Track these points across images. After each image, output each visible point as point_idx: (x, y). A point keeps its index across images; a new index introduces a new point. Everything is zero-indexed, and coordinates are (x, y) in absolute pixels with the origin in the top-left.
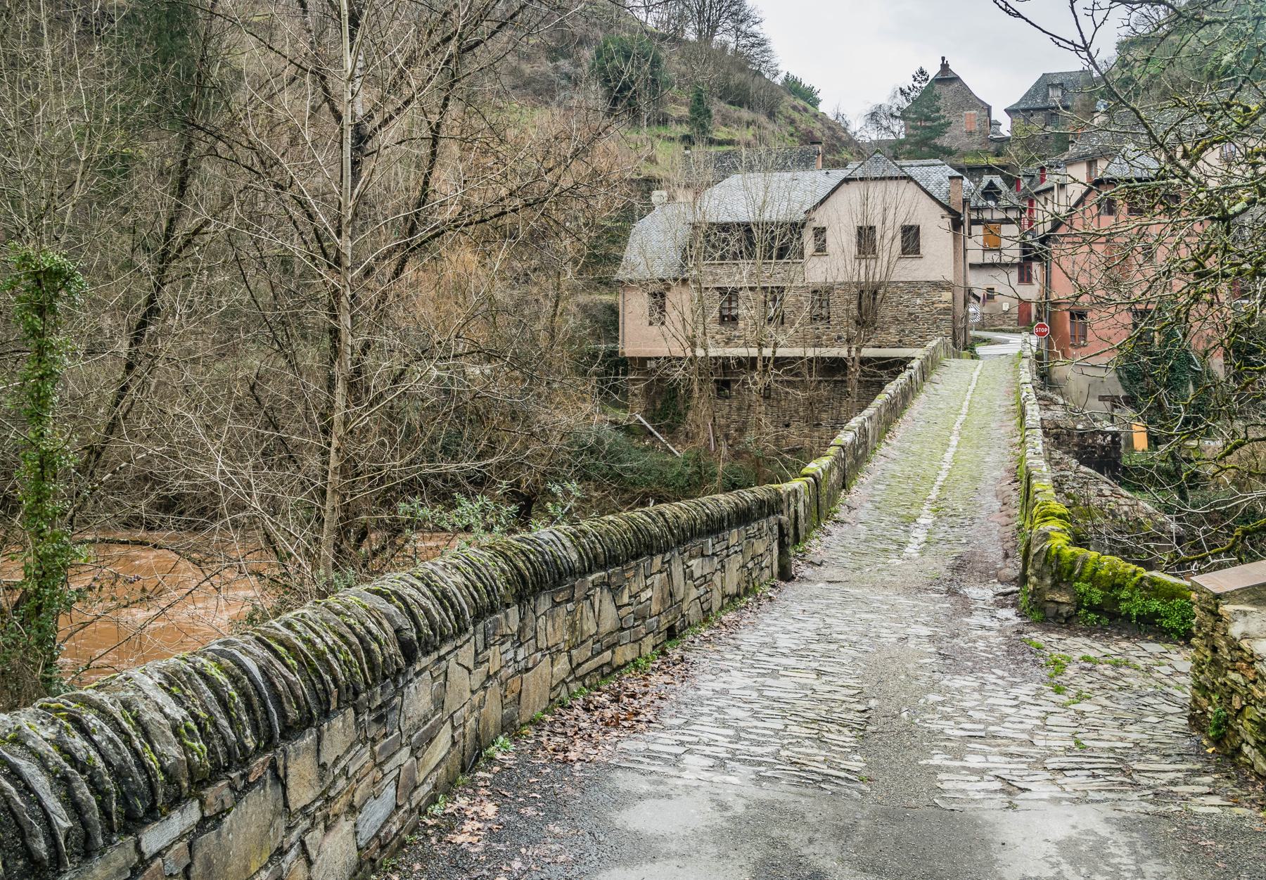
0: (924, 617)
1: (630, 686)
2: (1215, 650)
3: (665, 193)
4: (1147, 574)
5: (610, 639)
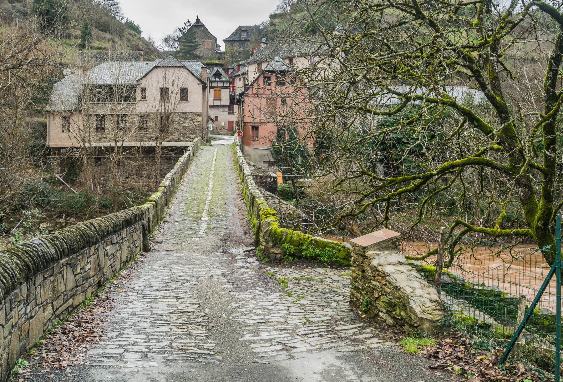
0: (216, 265)
1: (83, 316)
2: (363, 271)
3: (70, 70)
4: (313, 238)
5: (72, 293)
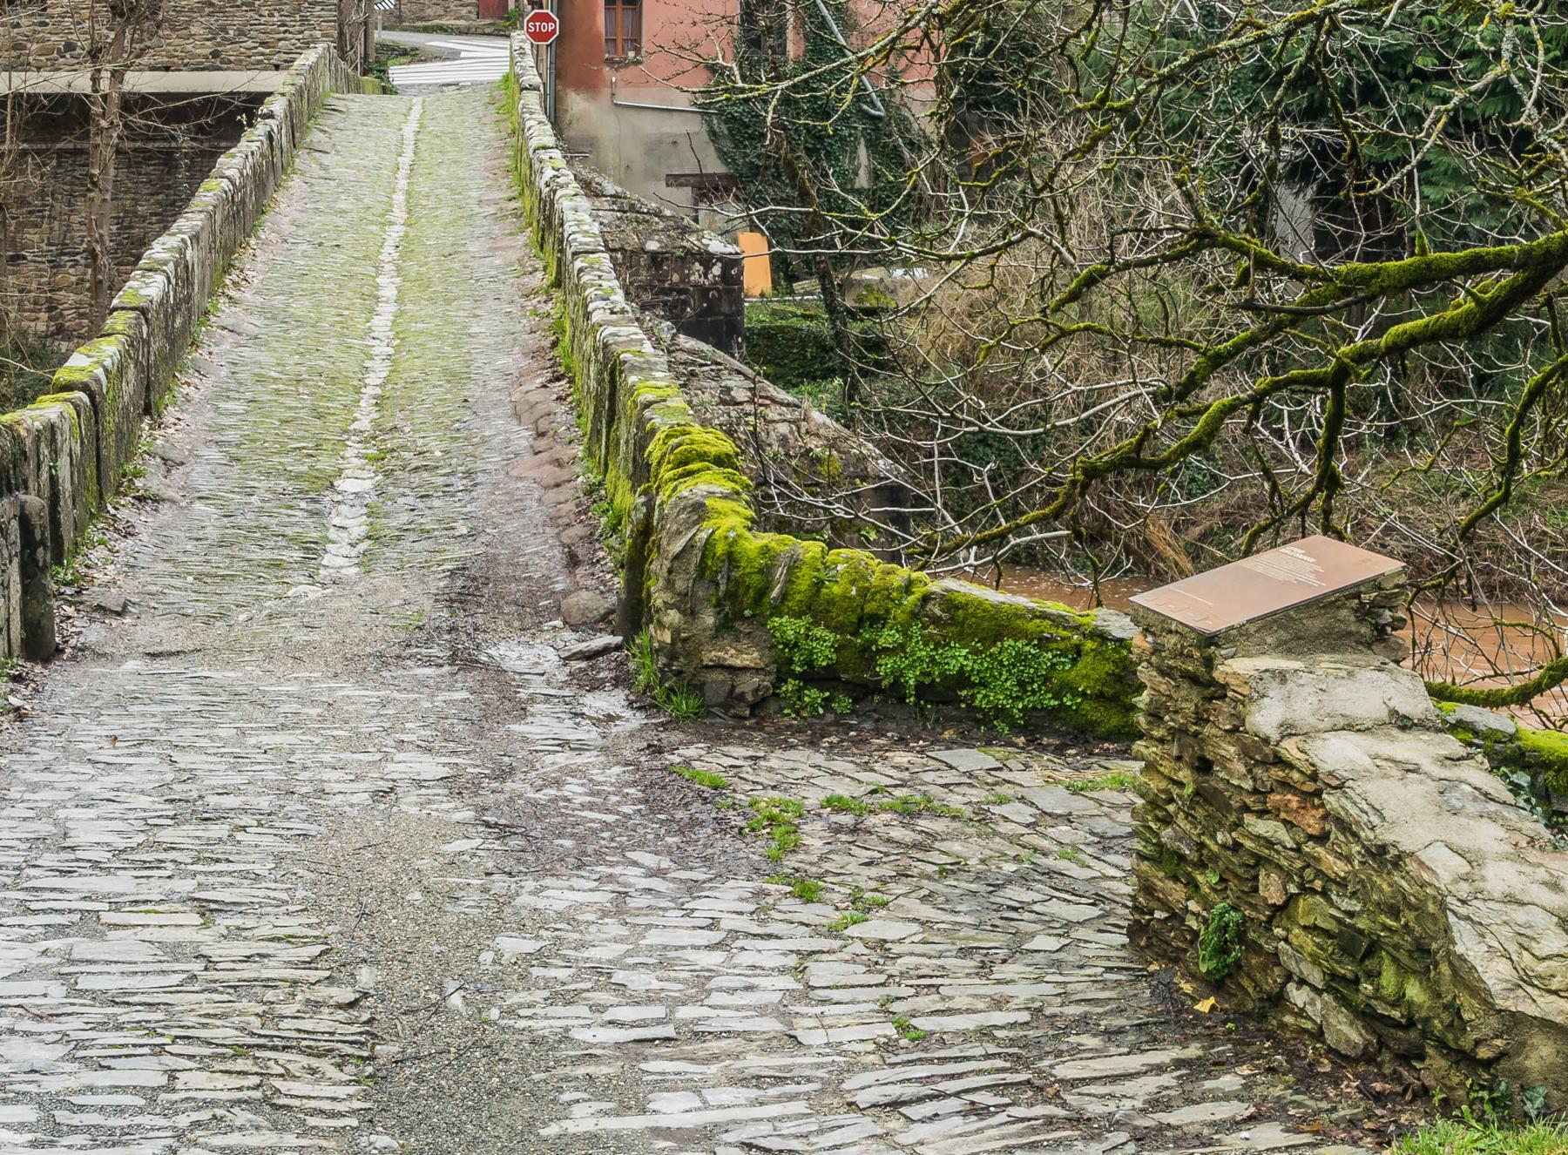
0: (414, 732)
2: (1204, 766)
4: (935, 587)
